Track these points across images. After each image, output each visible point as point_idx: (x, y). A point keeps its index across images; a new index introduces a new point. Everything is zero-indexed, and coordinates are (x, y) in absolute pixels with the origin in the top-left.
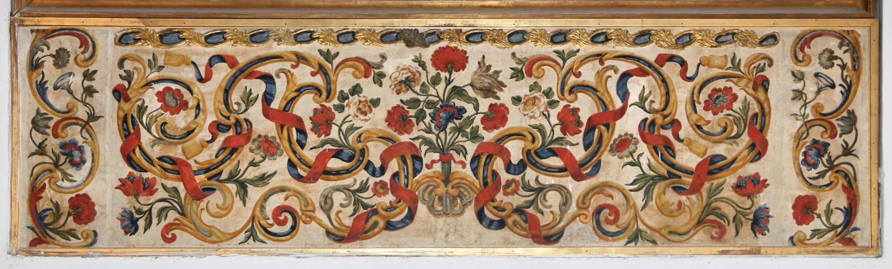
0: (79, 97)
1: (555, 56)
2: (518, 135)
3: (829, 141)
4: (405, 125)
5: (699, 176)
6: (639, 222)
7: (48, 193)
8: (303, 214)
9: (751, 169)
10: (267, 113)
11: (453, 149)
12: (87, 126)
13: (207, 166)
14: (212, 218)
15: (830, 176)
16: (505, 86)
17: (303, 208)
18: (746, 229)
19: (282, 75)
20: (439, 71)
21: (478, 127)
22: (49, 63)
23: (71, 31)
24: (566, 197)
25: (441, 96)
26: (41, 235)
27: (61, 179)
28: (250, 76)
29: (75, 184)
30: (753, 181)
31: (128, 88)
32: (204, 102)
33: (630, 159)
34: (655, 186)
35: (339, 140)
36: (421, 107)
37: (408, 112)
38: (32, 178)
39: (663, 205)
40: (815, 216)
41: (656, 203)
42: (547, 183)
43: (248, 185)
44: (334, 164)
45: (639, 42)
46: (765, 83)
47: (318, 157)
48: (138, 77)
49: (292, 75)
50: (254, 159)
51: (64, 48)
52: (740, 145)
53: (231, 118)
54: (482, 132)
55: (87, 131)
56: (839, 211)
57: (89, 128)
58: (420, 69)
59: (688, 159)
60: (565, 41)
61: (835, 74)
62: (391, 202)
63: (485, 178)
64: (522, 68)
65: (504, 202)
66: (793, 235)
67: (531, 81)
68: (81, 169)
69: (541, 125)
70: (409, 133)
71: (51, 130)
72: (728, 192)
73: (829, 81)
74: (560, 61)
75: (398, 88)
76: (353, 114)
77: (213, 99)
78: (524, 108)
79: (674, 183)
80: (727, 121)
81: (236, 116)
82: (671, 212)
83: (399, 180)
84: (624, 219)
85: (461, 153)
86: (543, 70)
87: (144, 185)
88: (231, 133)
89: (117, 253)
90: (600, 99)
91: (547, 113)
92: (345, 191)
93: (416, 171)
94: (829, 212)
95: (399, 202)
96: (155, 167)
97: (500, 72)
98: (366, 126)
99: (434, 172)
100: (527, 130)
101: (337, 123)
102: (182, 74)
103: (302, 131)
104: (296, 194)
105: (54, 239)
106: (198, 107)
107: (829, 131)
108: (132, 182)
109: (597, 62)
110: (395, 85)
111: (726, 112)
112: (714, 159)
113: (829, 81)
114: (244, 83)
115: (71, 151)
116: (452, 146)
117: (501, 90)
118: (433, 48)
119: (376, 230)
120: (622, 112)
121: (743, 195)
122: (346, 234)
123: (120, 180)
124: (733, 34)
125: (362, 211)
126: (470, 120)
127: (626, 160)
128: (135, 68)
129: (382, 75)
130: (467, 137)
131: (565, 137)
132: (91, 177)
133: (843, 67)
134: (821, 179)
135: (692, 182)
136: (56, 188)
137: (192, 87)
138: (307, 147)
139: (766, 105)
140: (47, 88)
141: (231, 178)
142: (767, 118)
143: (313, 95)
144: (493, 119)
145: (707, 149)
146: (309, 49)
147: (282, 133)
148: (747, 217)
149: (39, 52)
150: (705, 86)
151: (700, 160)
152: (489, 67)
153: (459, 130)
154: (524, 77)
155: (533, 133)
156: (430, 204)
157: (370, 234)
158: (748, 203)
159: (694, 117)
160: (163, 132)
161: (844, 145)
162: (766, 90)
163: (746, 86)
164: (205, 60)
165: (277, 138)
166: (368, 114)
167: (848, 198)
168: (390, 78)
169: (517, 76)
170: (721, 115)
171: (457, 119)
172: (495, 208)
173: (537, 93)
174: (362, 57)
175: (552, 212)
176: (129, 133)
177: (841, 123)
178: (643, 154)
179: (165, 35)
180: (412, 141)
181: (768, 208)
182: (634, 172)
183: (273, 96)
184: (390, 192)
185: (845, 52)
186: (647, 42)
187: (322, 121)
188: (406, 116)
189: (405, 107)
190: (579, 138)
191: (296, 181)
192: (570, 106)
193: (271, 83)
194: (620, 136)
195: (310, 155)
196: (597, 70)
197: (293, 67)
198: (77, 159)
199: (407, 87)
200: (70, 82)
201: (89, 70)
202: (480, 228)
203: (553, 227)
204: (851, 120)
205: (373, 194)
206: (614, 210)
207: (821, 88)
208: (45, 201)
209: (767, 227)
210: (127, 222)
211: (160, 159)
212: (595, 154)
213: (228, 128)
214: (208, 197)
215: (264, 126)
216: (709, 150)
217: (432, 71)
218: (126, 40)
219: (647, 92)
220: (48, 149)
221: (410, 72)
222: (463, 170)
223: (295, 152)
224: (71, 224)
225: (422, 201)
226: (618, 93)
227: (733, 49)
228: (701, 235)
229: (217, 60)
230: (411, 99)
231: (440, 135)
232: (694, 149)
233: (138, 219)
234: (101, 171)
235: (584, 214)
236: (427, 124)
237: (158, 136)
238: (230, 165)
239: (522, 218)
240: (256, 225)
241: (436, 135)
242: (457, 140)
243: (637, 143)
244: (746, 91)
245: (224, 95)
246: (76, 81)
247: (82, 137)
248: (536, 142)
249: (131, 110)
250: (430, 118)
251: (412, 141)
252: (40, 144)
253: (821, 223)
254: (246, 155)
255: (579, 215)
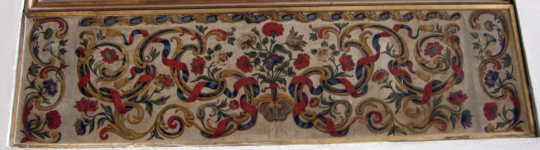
0: (56, 55)
1: (334, 26)
2: (316, 71)
3: (498, 71)
4: (248, 67)
5: (427, 93)
6: (395, 121)
7: (35, 110)
8: (186, 121)
9: (456, 88)
10: (165, 61)
11: (277, 81)
12: (60, 71)
13: (128, 93)
14: (130, 125)
15: (502, 91)
16: (307, 44)
17: (187, 117)
18: (459, 124)
19: (174, 40)
20: (267, 36)
21: (292, 67)
22: (41, 36)
23: (55, 19)
25: (269, 49)
26: (28, 136)
27: (42, 102)
28: (156, 41)
29: (50, 105)
30: (459, 95)
31: (85, 49)
32: (128, 56)
33: (385, 84)
35: (208, 76)
36: (257, 56)
37: (249, 60)
38: (26, 102)
39: (408, 110)
40: (497, 115)
41: (403, 109)
42: (336, 99)
43: (153, 104)
44: (205, 90)
46: (457, 39)
47: (196, 87)
48: (91, 43)
49: (180, 40)
50: (157, 88)
51: (50, 29)
53: (143, 65)
54: (294, 70)
55: (60, 74)
56: (510, 112)
57: (60, 72)
58: (256, 35)
59: (419, 83)
60: (340, 18)
61: (495, 34)
62: (241, 113)
63: (298, 97)
64: (316, 33)
65: (311, 111)
66: (486, 126)
67: (322, 40)
68: (54, 96)
69: (330, 65)
70: (250, 72)
71: (39, 74)
72: (445, 102)
73: (493, 38)
74: (338, 30)
75: (243, 46)
76: (216, 61)
77: (133, 55)
78: (319, 56)
79: (412, 97)
80: (438, 61)
81: (147, 64)
82: (413, 115)
83: (245, 100)
84: (386, 119)
86: (328, 34)
87: (91, 105)
88: (143, 74)
89: (72, 146)
90: (363, 50)
92: (213, 107)
93: (256, 94)
94: (505, 113)
95: (246, 112)
97: (303, 36)
98: (224, 68)
99: (267, 94)
100: (322, 68)
101: (207, 66)
102: (116, 41)
103: (186, 72)
105: (36, 138)
106: (124, 59)
108: (84, 103)
109: (359, 29)
110: (241, 45)
111: (437, 56)
112: (434, 83)
113: (493, 38)
114: (152, 45)
116: (277, 79)
117: (305, 46)
118: (262, 24)
119: (232, 130)
120: (377, 57)
121: (455, 104)
122: (213, 133)
123: (77, 102)
124: (436, 13)
125: (223, 118)
126: (287, 64)
127: (383, 85)
128: (90, 38)
129: (233, 39)
130: (286, 74)
131: (345, 72)
132: (60, 101)
133: (499, 30)
134: (497, 93)
135: (423, 97)
137: (121, 48)
138: (189, 81)
139: (459, 52)
140: (39, 50)
141: (143, 100)
142: (461, 58)
144: (301, 63)
145: (429, 77)
146: (192, 26)
147: (174, 73)
148: (458, 116)
149: (37, 31)
151: (426, 83)
152: (296, 33)
153: (281, 69)
155: (325, 70)
157: (228, 132)
158: (458, 109)
159: (420, 59)
160: (104, 74)
161: (507, 73)
163: (447, 41)
164: (130, 33)
165: (171, 76)
166: (225, 61)
167: (514, 104)
168: (238, 40)
169: (313, 38)
170: (435, 58)
171: (279, 63)
172: (305, 115)
173: (326, 47)
174: (221, 29)
175: (341, 117)
179: (107, 20)
181: (469, 111)
183: (168, 52)
184: (240, 107)
185: (498, 22)
186: (387, 18)
187: (198, 66)
188: (248, 62)
189: (248, 57)
190: (353, 73)
191: (182, 102)
193: (168, 45)
194: (378, 71)
195: (191, 85)
196: (360, 34)
197: (181, 35)
198: (52, 90)
201: (63, 40)
202: (298, 128)
203: (342, 126)
204: (508, 60)
205: (230, 108)
207: (489, 42)
208: (32, 115)
209: (470, 122)
210: (79, 127)
211: (101, 89)
212: (364, 81)
213: (142, 70)
214: (128, 112)
215: (163, 69)
217: (263, 36)
218: (85, 23)
219: (390, 46)
220: (37, 85)
221: (250, 37)
222: (284, 93)
223: (181, 84)
224: (46, 129)
225: (260, 112)
226: (374, 47)
227: (436, 21)
228: (432, 128)
229: (136, 33)
230: (251, 52)
232: (422, 77)
233: (86, 126)
234: (66, 97)
235: (360, 118)
236: (261, 66)
237: (100, 76)
238: (143, 92)
239: (323, 121)
240: (158, 128)
241: (267, 72)
242: (280, 75)
243: (388, 74)
244: (447, 44)
245: (140, 52)
246: (55, 46)
248: (328, 75)
249: (85, 61)
250: (263, 63)
251: (252, 76)
252: (32, 82)
253: (501, 119)
254: (152, 86)
255: (358, 118)
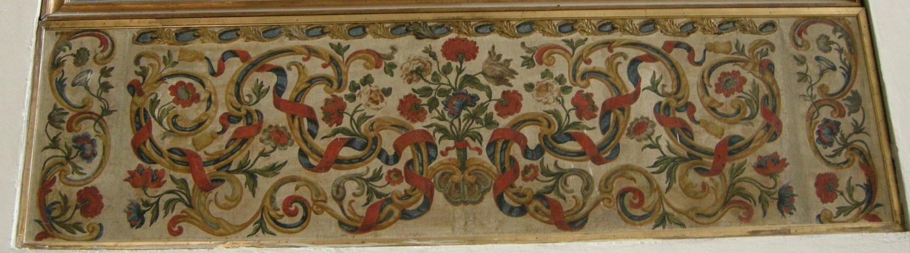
1: (563, 45)
2: (533, 120)
3: (839, 119)
4: (418, 113)
5: (719, 157)
6: (665, 205)
7: (58, 186)
8: (314, 204)
9: (769, 149)
10: (279, 104)
11: (467, 136)
12: (101, 120)
13: (216, 157)
14: (220, 210)
15: (846, 154)
16: (517, 74)
17: (315, 198)
18: (773, 208)
19: (293, 67)
20: (450, 61)
21: (492, 114)
22: (69, 61)
23: (92, 32)
24: (588, 181)
26: (47, 229)
27: (71, 172)
28: (262, 69)
29: (84, 177)
30: (773, 160)
31: (143, 83)
32: (216, 94)
33: (649, 142)
34: (676, 168)
35: (351, 129)
36: (433, 95)
37: (420, 101)
38: (44, 171)
39: (687, 186)
40: (838, 194)
42: (567, 167)
43: (257, 175)
44: (346, 152)
45: (645, 31)
47: (330, 147)
48: (153, 72)
50: (264, 149)
51: (84, 48)
52: (755, 125)
54: (496, 118)
55: (101, 125)
58: (431, 59)
59: (706, 140)
60: (573, 30)
61: (834, 57)
62: (405, 191)
63: (502, 164)
64: (532, 56)
66: (820, 213)
67: (543, 68)
68: (91, 161)
69: (556, 110)
70: (422, 121)
71: (66, 124)
72: (749, 172)
74: (570, 50)
75: (410, 77)
76: (364, 103)
78: (538, 94)
79: (694, 164)
81: (248, 107)
83: (413, 168)
84: (650, 201)
85: (476, 140)
86: (553, 58)
87: (153, 177)
88: (241, 124)
89: (121, 246)
90: (613, 84)
91: (560, 99)
92: (358, 180)
93: (431, 159)
94: (850, 190)
95: (414, 190)
96: (164, 158)
97: (511, 60)
98: (378, 115)
99: (450, 159)
100: (542, 115)
103: (313, 121)
104: (307, 184)
106: (209, 100)
107: (837, 111)
109: (606, 49)
110: (407, 75)
111: (737, 94)
112: (732, 140)
113: (830, 64)
115: (84, 144)
116: (467, 133)
117: (513, 78)
118: (442, 40)
119: (391, 220)
120: (636, 96)
121: (765, 175)
122: (360, 225)
123: (129, 172)
124: (734, 22)
125: (375, 200)
126: (483, 107)
128: (151, 65)
129: (393, 66)
130: (482, 124)
131: (582, 121)
132: (100, 170)
133: (841, 51)
134: (837, 157)
136: (65, 181)
137: (205, 81)
138: (319, 137)
139: (774, 87)
140: (66, 85)
141: (241, 169)
142: (777, 99)
143: (324, 86)
146: (323, 43)
148: (772, 196)
149: (62, 52)
150: (713, 70)
151: (718, 141)
152: (499, 56)
153: (473, 117)
154: (534, 64)
156: (447, 192)
158: (771, 183)
159: (707, 99)
160: (175, 124)
162: (773, 73)
164: (219, 55)
165: (288, 128)
167: (866, 175)
168: (401, 68)
169: (528, 64)
170: (733, 97)
172: (514, 194)
173: (549, 79)
174: (372, 49)
175: (574, 197)
176: (141, 126)
177: (848, 103)
178: (661, 136)
179: (181, 33)
180: (425, 129)
181: (791, 187)
182: (654, 155)
184: (404, 180)
185: (840, 37)
187: (334, 111)
189: (418, 96)
190: (595, 122)
192: (583, 91)
194: (636, 119)
195: (321, 144)
196: (607, 57)
197: (304, 60)
198: (88, 152)
199: (419, 76)
200: (88, 78)
201: (106, 67)
202: (501, 216)
204: (856, 101)
205: (387, 183)
206: (638, 193)
207: (824, 70)
208: (55, 194)
209: (793, 206)
210: (134, 215)
211: (170, 150)
212: (613, 137)
213: (239, 119)
214: (216, 189)
215: (275, 117)
216: (726, 131)
217: (443, 61)
219: (657, 77)
220: (62, 143)
221: (421, 62)
222: (479, 157)
223: (306, 142)
224: (78, 217)
225: (437, 189)
228: (729, 216)
229: (229, 55)
230: (423, 88)
231: (454, 122)
233: (144, 212)
234: (111, 164)
236: (440, 111)
237: (168, 129)
241: (450, 122)
242: (471, 127)
243: (653, 125)
244: (754, 75)
246: (93, 78)
247: (95, 130)
248: (552, 127)
250: (443, 106)
251: (425, 129)
252: (55, 138)
254: (257, 145)
255: (603, 199)
